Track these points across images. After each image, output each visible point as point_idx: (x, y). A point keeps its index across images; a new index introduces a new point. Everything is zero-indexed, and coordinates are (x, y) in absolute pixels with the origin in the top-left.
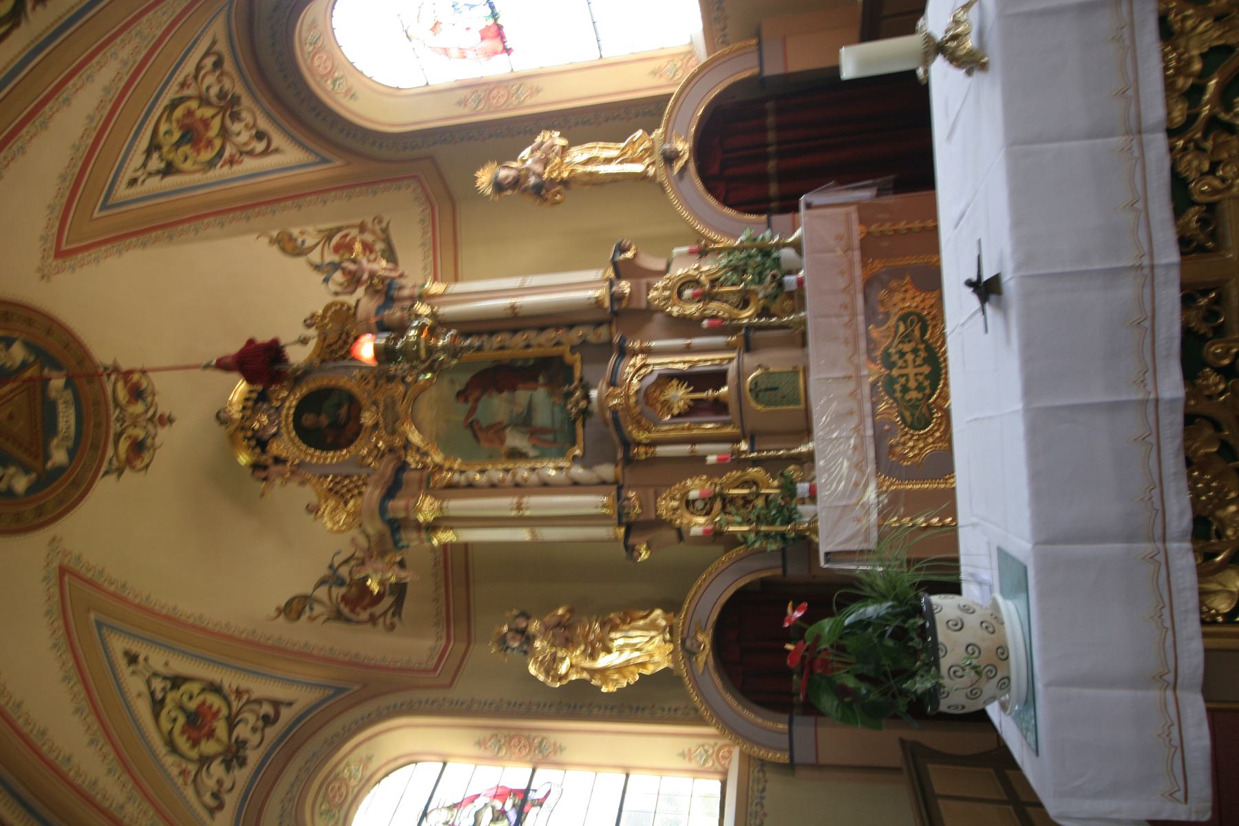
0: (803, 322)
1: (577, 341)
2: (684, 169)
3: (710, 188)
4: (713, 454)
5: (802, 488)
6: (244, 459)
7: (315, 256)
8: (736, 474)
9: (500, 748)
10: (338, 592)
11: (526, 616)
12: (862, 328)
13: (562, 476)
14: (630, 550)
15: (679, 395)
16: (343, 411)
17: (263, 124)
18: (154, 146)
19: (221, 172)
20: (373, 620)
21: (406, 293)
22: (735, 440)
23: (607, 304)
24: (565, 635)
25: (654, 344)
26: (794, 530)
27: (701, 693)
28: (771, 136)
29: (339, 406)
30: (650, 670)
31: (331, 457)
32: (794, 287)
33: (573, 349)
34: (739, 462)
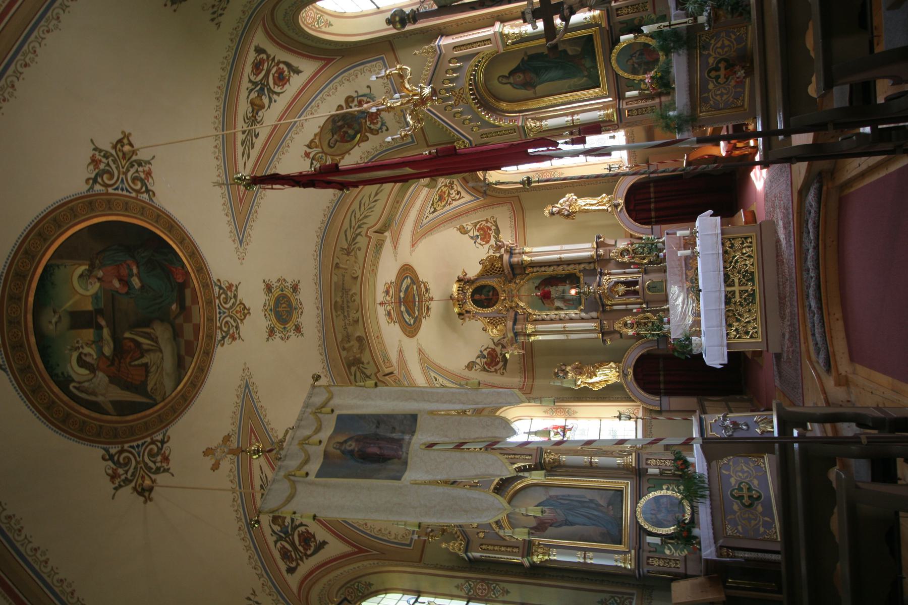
0: (666, 266)
1: (582, 269)
2: (621, 209)
3: (630, 216)
4: (635, 308)
5: (665, 320)
6: (456, 310)
7: (471, 234)
8: (642, 315)
9: (553, 414)
10: (484, 360)
11: (565, 365)
12: (684, 272)
13: (577, 316)
14: (604, 341)
15: (622, 289)
16: (491, 294)
17: (460, 189)
18: (433, 204)
19: (447, 208)
20: (496, 371)
21: (517, 251)
22: (642, 304)
23: (595, 257)
24: (579, 371)
25: (612, 271)
26: (663, 333)
27: (629, 388)
28: (652, 195)
29: (489, 292)
30: (610, 383)
31: (487, 311)
32: (663, 257)
33: (580, 272)
34: (644, 312)
